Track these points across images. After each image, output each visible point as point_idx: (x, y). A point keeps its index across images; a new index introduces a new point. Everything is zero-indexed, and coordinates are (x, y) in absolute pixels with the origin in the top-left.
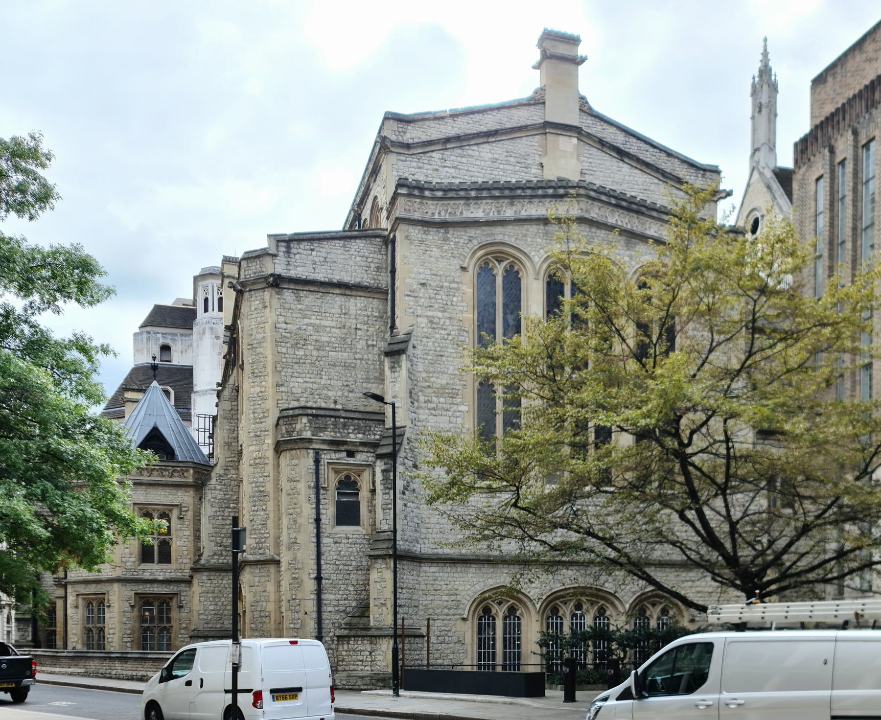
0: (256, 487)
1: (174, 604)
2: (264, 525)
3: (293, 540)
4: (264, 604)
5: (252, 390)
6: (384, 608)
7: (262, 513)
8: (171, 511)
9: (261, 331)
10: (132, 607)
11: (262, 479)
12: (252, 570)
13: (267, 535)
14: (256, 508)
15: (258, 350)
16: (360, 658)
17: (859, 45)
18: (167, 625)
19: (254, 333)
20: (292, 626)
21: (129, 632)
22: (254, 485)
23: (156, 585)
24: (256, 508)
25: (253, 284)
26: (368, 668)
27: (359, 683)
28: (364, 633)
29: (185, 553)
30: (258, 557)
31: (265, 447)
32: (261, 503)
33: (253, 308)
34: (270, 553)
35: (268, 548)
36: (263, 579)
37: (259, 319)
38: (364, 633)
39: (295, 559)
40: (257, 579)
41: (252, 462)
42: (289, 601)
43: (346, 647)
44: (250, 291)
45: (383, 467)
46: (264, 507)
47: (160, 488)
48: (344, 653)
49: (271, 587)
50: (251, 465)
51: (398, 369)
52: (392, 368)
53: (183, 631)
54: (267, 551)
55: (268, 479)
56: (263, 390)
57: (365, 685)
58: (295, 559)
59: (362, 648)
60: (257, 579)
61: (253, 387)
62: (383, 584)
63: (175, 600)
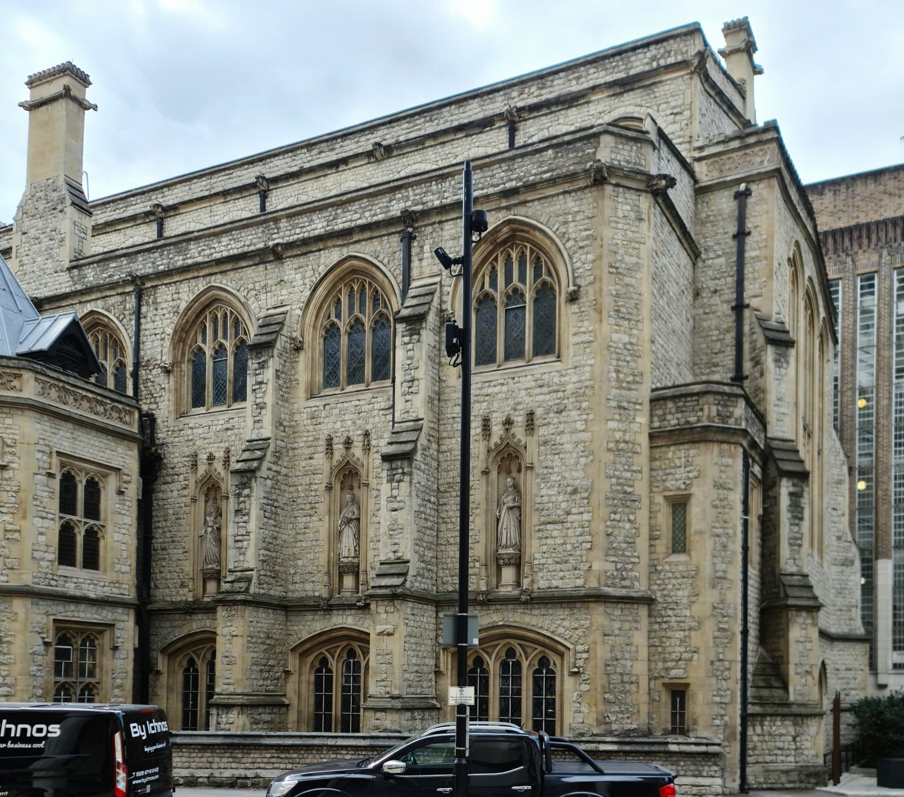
0: (620, 484)
1: (105, 641)
2: (631, 544)
3: (720, 574)
4: (629, 663)
5: (615, 337)
6: (809, 678)
7: (628, 526)
8: (106, 476)
9: (634, 252)
10: (47, 644)
11: (628, 475)
12: (609, 610)
13: (636, 560)
14: (618, 517)
15: (627, 280)
16: (780, 745)
17: (876, 175)
18: (92, 680)
19: (621, 251)
20: (717, 699)
21: (40, 692)
22: (614, 481)
23: (82, 607)
24: (618, 517)
25: (626, 177)
26: (791, 759)
27: (784, 779)
28: (785, 710)
29: (125, 554)
30: (624, 592)
31: (635, 427)
32: (627, 510)
33: (620, 214)
34: (640, 588)
35: (637, 579)
36: (627, 626)
37: (630, 234)
38: (781, 710)
39: (722, 601)
40: (617, 625)
41: (611, 445)
42: (712, 663)
43: (758, 730)
44: (617, 185)
45: (792, 489)
46: (632, 517)
47: (93, 433)
48: (755, 738)
49: (640, 639)
50: (609, 450)
51: (785, 365)
52: (777, 361)
53: (117, 691)
54: (636, 584)
55: (639, 476)
56: (634, 341)
57: (790, 782)
58: (722, 601)
59: (784, 731)
60: (617, 625)
61: (616, 332)
62: (809, 645)
63: (107, 635)
